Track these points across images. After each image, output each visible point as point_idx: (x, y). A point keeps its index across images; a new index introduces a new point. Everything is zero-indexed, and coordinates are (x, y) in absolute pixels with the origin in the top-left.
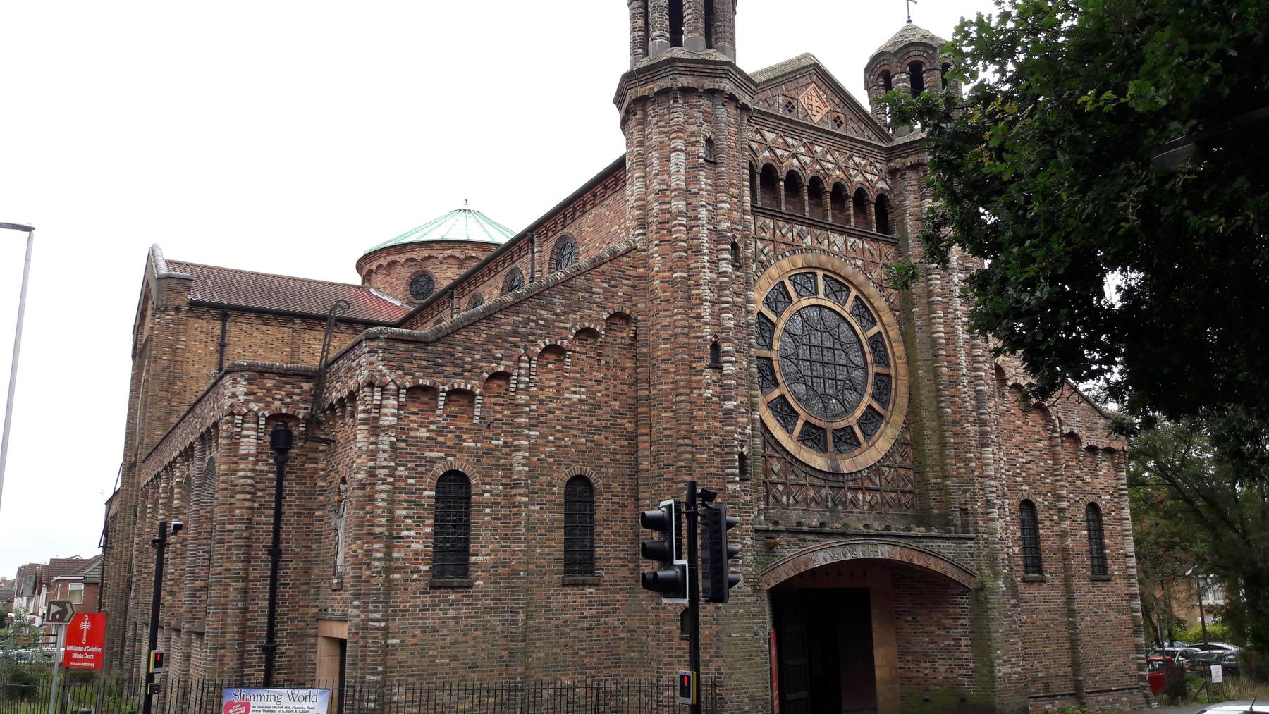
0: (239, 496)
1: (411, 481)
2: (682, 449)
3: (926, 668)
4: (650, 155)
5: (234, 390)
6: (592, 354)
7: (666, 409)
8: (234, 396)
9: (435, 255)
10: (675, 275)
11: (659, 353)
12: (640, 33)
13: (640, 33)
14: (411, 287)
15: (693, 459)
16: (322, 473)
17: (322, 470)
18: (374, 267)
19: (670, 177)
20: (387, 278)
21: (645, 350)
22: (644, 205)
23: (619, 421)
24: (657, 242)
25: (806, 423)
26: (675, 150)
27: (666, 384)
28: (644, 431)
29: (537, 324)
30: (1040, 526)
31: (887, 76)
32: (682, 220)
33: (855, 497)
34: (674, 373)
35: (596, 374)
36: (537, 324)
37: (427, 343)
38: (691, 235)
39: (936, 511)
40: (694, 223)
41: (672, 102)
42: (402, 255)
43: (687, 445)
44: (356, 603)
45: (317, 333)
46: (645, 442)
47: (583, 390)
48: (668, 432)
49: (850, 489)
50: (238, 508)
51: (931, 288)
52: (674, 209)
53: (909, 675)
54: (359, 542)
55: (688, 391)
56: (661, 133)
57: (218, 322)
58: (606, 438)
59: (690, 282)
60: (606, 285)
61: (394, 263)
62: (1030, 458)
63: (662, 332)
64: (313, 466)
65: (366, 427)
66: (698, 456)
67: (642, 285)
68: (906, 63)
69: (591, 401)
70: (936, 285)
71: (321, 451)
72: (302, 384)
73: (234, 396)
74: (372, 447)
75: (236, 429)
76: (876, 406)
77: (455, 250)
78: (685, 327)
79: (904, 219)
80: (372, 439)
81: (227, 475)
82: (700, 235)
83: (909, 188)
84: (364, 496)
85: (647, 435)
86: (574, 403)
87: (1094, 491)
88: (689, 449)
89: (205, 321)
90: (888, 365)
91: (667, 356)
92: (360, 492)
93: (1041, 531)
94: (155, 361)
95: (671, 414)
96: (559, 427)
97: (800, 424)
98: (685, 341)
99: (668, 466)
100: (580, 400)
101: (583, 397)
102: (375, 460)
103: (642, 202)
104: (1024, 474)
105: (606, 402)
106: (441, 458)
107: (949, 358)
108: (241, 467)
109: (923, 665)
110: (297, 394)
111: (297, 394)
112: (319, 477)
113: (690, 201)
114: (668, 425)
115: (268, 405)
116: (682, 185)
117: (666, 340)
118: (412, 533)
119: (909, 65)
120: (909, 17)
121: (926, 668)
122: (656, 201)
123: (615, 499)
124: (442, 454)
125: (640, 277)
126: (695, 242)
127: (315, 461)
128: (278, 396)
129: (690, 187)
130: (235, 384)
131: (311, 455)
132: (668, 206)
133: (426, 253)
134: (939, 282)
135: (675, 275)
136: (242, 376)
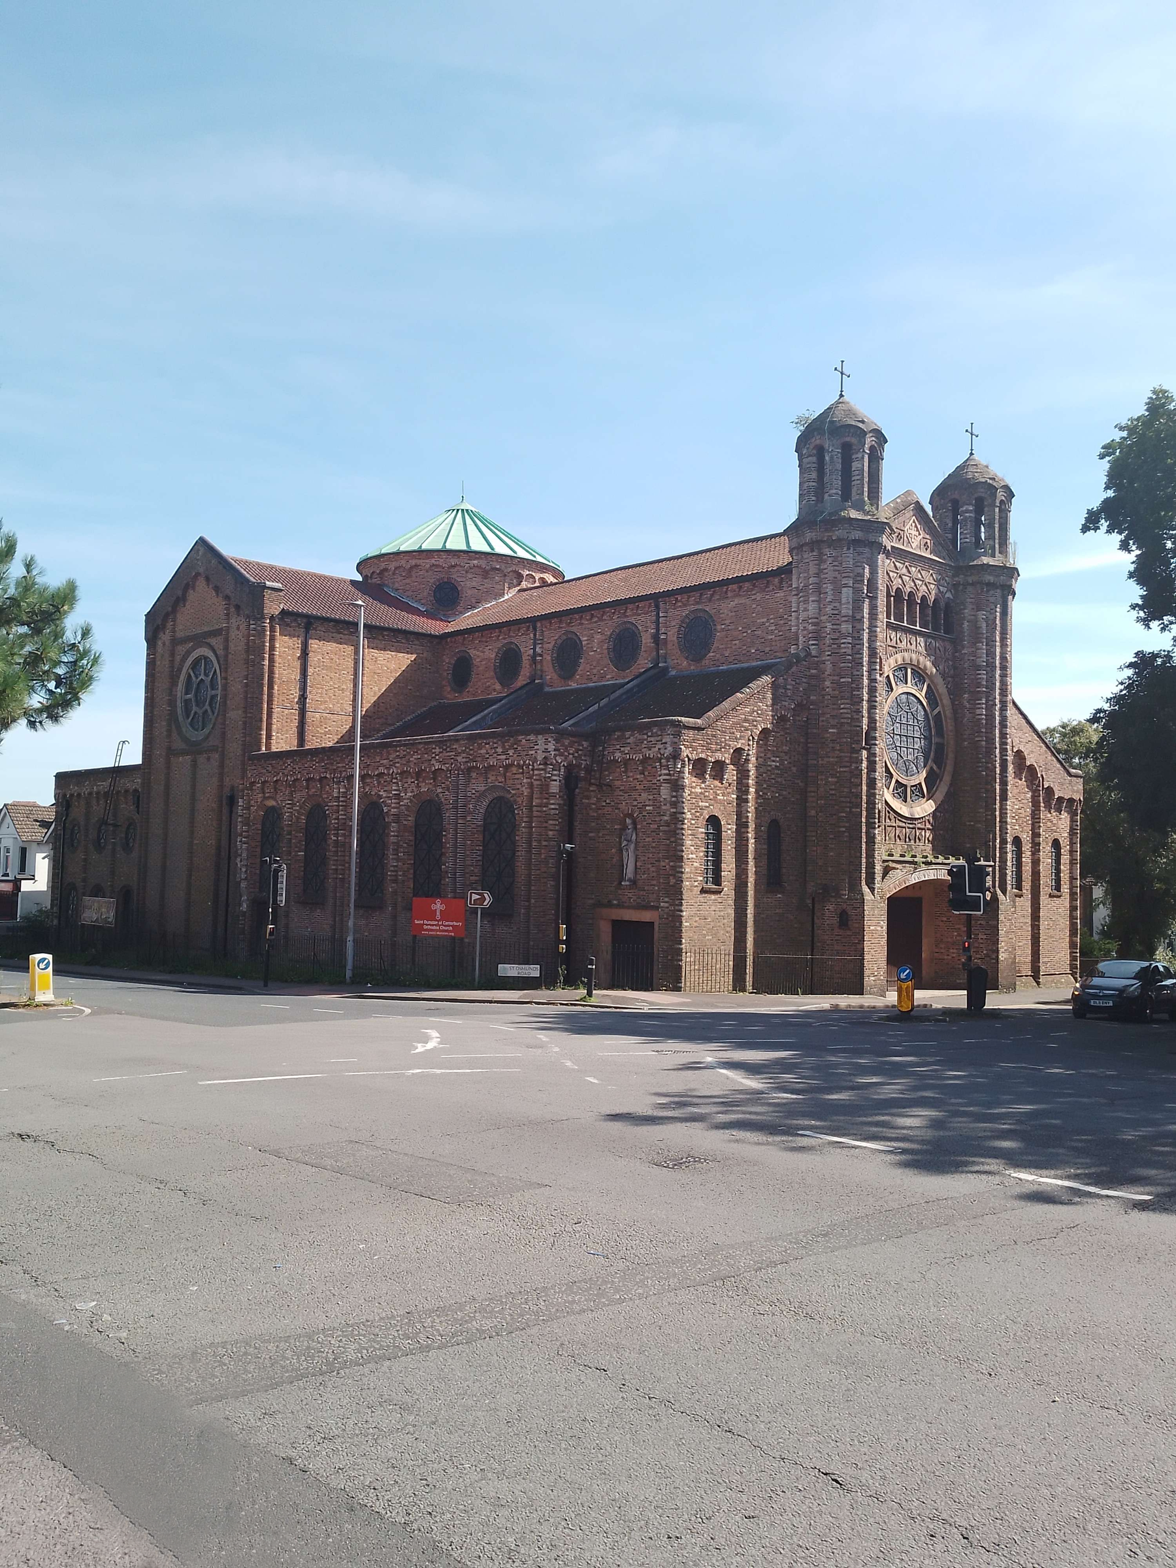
0: (551, 822)
1: (693, 822)
2: (844, 805)
3: (953, 953)
4: (824, 586)
5: (546, 747)
6: (782, 733)
7: (833, 776)
8: (546, 751)
9: (462, 564)
10: (842, 680)
11: (828, 735)
12: (814, 484)
13: (814, 484)
14: (435, 592)
15: (851, 812)
16: (594, 806)
17: (594, 804)
18: (392, 566)
19: (841, 605)
20: (407, 581)
21: (815, 731)
22: (818, 623)
23: (796, 781)
24: (830, 653)
25: (897, 781)
26: (846, 586)
27: (833, 757)
28: (812, 789)
29: (758, 714)
30: (1023, 855)
31: (956, 506)
32: (850, 640)
33: (920, 834)
34: (839, 750)
35: (784, 747)
36: (758, 714)
37: (703, 729)
38: (855, 650)
39: (968, 845)
40: (857, 642)
41: (845, 549)
42: (427, 561)
43: (847, 802)
44: (666, 899)
45: (378, 642)
46: (813, 797)
47: (778, 759)
48: (833, 792)
49: (919, 829)
50: (551, 830)
51: (979, 681)
52: (844, 631)
53: (941, 957)
54: (667, 861)
55: (848, 764)
56: (835, 571)
57: (303, 630)
58: (789, 793)
59: (853, 685)
60: (794, 683)
61: (416, 566)
62: (1021, 805)
63: (831, 720)
64: (587, 801)
65: (669, 785)
66: (854, 810)
67: (813, 682)
68: (974, 497)
69: (781, 767)
70: (983, 678)
71: (592, 791)
72: (584, 743)
73: (546, 751)
74: (673, 799)
75: (548, 775)
76: (935, 767)
77: (481, 561)
78: (849, 718)
79: (963, 624)
80: (674, 794)
81: (540, 806)
82: (861, 652)
83: (969, 600)
84: (670, 831)
85: (814, 792)
86: (773, 769)
87: (1058, 830)
88: (848, 805)
89: (292, 629)
90: (943, 737)
91: (834, 738)
92: (666, 828)
93: (1023, 859)
94: (253, 666)
95: (836, 780)
96: (765, 786)
97: (894, 781)
98: (849, 728)
99: (832, 815)
100: (776, 766)
101: (778, 764)
102: (676, 808)
103: (816, 620)
104: (1017, 817)
105: (790, 768)
106: (707, 807)
107: (987, 735)
108: (551, 802)
109: (951, 951)
110: (581, 750)
111: (581, 750)
112: (591, 809)
113: (855, 625)
114: (833, 787)
115: (566, 757)
116: (850, 613)
117: (833, 727)
118: (694, 856)
119: (976, 499)
120: (972, 450)
121: (953, 953)
122: (829, 622)
123: (793, 836)
124: (707, 804)
125: (812, 676)
126: (858, 656)
127: (588, 798)
128: (571, 752)
129: (856, 615)
130: (547, 742)
131: (586, 794)
132: (838, 627)
133: (413, 562)
134: (985, 677)
135: (842, 680)
136: (552, 737)
